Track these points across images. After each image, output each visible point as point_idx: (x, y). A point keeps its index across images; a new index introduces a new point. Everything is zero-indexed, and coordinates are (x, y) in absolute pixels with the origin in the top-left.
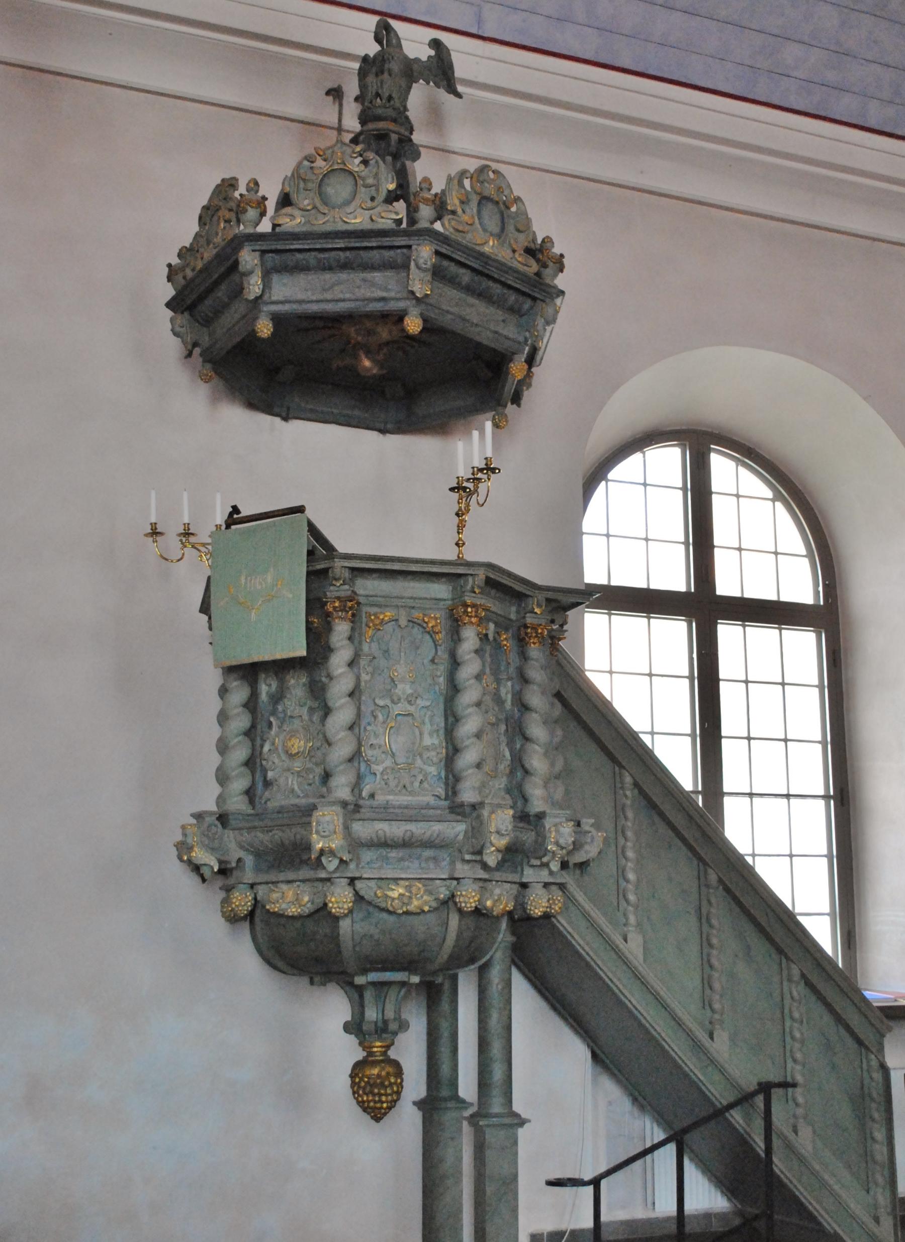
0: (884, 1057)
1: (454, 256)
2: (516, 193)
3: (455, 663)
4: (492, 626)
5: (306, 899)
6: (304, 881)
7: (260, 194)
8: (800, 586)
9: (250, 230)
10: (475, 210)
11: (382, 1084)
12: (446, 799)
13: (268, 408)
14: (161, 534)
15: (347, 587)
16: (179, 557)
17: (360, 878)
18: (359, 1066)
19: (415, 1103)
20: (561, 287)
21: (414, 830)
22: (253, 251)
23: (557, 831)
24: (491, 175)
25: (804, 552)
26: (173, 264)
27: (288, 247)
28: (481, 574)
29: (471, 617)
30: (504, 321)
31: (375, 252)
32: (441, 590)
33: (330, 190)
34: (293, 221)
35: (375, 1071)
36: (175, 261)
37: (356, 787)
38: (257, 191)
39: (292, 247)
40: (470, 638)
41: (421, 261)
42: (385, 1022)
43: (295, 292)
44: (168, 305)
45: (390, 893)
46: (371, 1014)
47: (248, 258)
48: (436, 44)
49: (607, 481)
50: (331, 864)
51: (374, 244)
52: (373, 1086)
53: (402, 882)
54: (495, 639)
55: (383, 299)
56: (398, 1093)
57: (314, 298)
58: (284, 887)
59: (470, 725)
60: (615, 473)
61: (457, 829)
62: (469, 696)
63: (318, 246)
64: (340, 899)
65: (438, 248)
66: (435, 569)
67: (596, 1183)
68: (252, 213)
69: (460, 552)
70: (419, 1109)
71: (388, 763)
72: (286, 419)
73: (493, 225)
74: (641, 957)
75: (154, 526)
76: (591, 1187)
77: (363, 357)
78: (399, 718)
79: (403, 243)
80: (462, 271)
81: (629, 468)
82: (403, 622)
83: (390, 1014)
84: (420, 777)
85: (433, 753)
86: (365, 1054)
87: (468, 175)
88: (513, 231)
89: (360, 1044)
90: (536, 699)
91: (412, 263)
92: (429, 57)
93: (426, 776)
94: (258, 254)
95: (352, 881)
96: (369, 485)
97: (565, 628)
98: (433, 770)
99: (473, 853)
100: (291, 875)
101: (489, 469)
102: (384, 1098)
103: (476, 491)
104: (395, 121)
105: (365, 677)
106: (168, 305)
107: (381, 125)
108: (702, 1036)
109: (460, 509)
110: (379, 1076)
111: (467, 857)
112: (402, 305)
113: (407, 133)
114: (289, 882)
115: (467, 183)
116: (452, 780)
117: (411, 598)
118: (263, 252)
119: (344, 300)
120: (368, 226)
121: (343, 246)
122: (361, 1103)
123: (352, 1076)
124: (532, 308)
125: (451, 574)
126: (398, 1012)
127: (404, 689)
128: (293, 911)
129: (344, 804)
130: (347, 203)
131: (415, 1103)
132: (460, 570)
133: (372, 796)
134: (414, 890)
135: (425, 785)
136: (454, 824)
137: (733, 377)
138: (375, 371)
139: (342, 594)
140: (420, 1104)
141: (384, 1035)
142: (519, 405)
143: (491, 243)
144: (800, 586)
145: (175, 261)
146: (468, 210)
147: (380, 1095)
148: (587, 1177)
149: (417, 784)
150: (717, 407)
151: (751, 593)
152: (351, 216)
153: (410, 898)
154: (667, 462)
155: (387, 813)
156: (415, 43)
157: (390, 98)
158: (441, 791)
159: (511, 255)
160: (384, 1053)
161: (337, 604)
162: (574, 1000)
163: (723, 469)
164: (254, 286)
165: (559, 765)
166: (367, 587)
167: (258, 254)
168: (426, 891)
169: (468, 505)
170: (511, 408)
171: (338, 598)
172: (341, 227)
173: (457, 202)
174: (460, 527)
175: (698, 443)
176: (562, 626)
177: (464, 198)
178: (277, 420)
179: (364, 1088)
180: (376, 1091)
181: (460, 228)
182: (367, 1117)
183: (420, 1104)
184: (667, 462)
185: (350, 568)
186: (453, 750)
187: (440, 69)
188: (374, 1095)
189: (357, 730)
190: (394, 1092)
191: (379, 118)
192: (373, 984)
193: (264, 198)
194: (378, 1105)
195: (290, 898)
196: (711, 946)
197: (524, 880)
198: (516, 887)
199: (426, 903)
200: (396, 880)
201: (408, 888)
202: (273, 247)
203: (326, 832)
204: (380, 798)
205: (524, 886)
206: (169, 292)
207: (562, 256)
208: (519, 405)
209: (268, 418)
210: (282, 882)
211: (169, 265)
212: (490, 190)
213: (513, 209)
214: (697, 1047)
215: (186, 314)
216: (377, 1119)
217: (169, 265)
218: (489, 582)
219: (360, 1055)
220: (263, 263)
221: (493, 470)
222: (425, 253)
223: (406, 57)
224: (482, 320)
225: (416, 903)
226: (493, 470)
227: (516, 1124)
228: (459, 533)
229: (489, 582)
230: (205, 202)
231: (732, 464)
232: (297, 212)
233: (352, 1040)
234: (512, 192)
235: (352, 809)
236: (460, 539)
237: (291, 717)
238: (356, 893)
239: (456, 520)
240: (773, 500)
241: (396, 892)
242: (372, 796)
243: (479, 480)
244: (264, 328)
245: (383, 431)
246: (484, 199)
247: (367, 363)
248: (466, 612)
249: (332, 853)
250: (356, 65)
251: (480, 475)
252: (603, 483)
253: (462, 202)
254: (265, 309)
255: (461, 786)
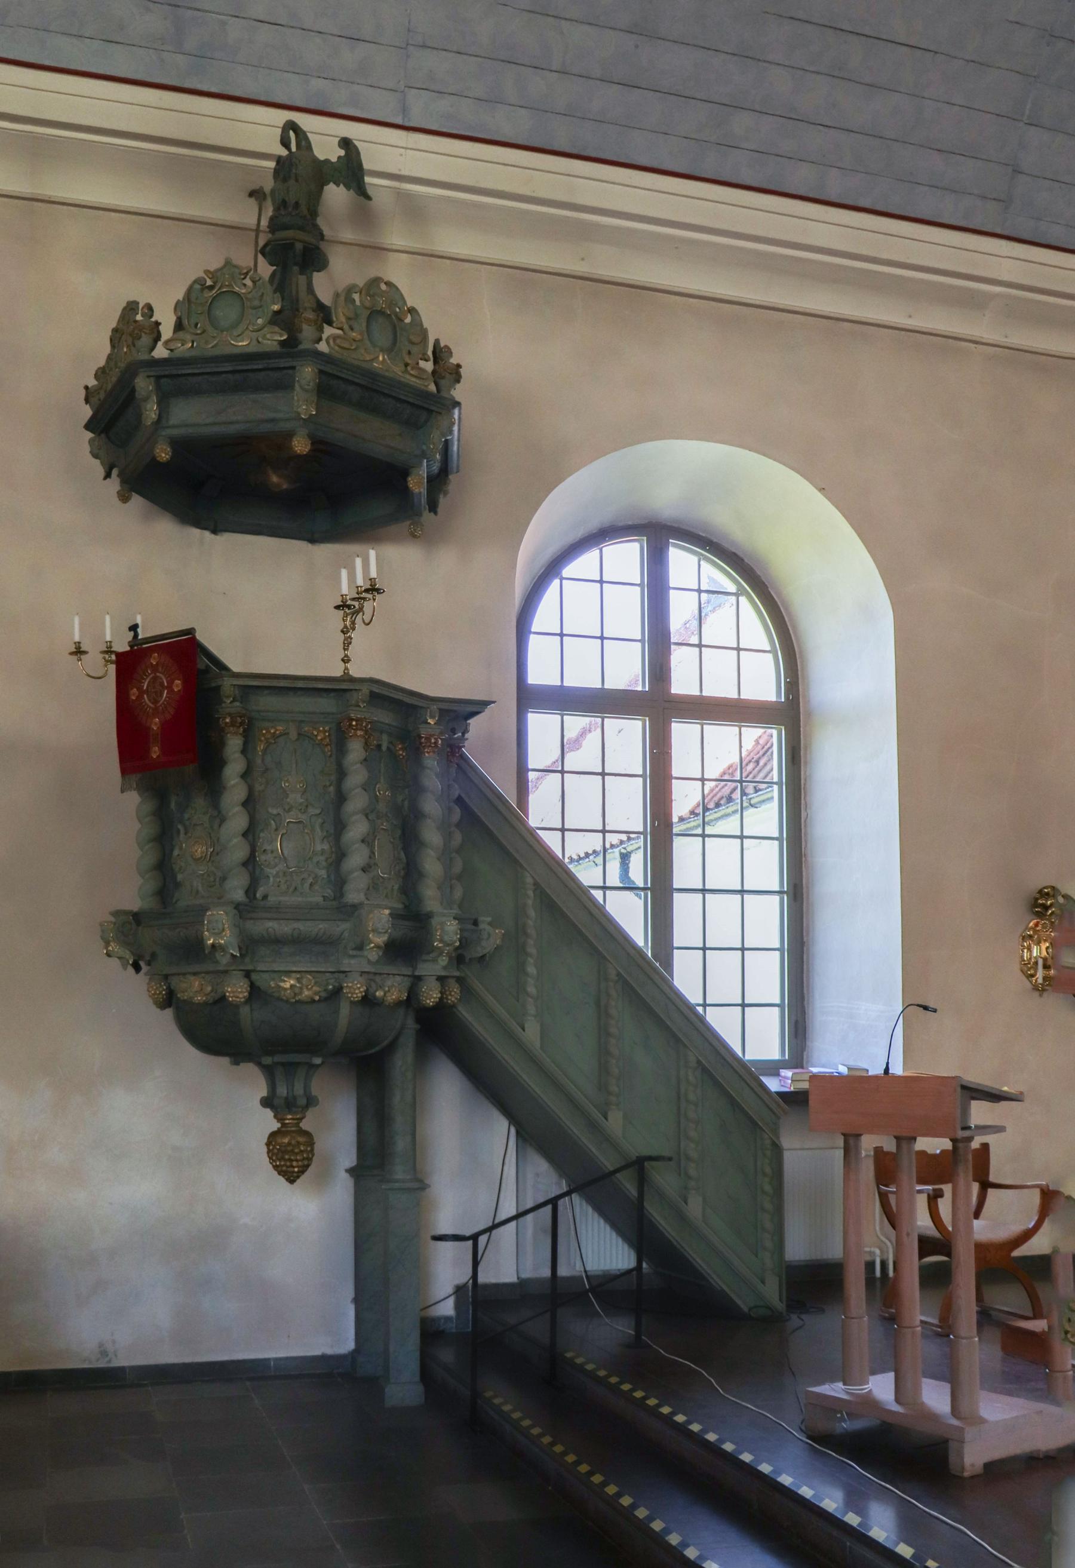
0: (778, 1138)
1: (339, 374)
2: (409, 304)
3: (342, 774)
4: (385, 737)
5: (209, 989)
6: (207, 973)
7: (153, 319)
8: (763, 683)
9: (144, 356)
10: (364, 324)
11: (292, 1151)
12: (335, 899)
13: (198, 524)
14: (85, 652)
15: (237, 704)
16: (100, 675)
17: (254, 971)
18: (273, 1135)
19: (347, 1171)
20: (457, 399)
21: (302, 928)
22: (148, 377)
23: (442, 929)
24: (383, 287)
25: (768, 648)
26: (90, 386)
27: (180, 372)
28: (365, 689)
29: (356, 730)
30: (400, 435)
31: (263, 373)
32: (326, 704)
33: (218, 313)
34: (184, 349)
35: (286, 1140)
36: (92, 382)
37: (250, 891)
38: (151, 316)
39: (184, 372)
40: (356, 751)
41: (303, 382)
42: (295, 1098)
43: (194, 416)
44: (88, 427)
45: (282, 984)
46: (282, 1091)
47: (143, 384)
48: (346, 143)
49: (562, 579)
50: (224, 960)
51: (260, 367)
52: (286, 1152)
53: (294, 975)
54: (388, 749)
55: (272, 420)
56: (310, 1159)
57: (207, 421)
58: (192, 978)
59: (357, 829)
60: (568, 571)
61: (343, 927)
62: (357, 802)
63: (208, 370)
64: (236, 990)
65: (322, 368)
66: (320, 686)
67: (475, 1238)
68: (145, 340)
69: (346, 668)
70: (351, 1176)
71: (282, 866)
72: (214, 532)
73: (382, 336)
74: (538, 1044)
75: (78, 645)
76: (470, 1242)
77: (270, 472)
78: (291, 825)
79: (287, 365)
80: (351, 388)
81: (585, 564)
82: (293, 735)
83: (299, 1090)
84: (310, 880)
85: (322, 858)
86: (279, 1125)
87: (357, 289)
88: (407, 343)
89: (275, 1117)
90: (431, 806)
91: (297, 385)
92: (339, 157)
93: (316, 877)
94: (152, 379)
95: (248, 974)
96: (267, 605)
97: (466, 736)
98: (323, 873)
99: (355, 949)
100: (197, 968)
101: (373, 589)
102: (295, 1164)
103: (361, 609)
104: (301, 228)
105: (258, 788)
106: (88, 427)
107: (290, 233)
108: (597, 1115)
109: (346, 627)
110: (289, 1144)
111: (351, 952)
112: (288, 426)
113: (313, 241)
114: (195, 974)
115: (356, 297)
116: (339, 883)
117: (301, 713)
118: (158, 378)
119: (237, 422)
120: (253, 349)
121: (230, 369)
122: (275, 1167)
123: (268, 1144)
124: (426, 421)
125: (339, 689)
126: (307, 1088)
127: (295, 798)
128: (199, 998)
129: (237, 906)
130: (235, 325)
131: (348, 1171)
132: (344, 686)
133: (265, 897)
134: (304, 981)
135: (316, 887)
136: (339, 923)
137: (681, 468)
138: (285, 486)
139: (232, 711)
140: (351, 1171)
141: (294, 1109)
142: (436, 513)
143: (381, 358)
144: (763, 683)
145: (92, 382)
146: (356, 326)
147: (291, 1160)
148: (468, 1233)
149: (307, 885)
150: (665, 500)
151: (711, 691)
152: (239, 339)
153: (301, 988)
154: (625, 557)
155: (278, 912)
156: (325, 138)
157: (297, 205)
158: (329, 892)
159: (403, 368)
160: (297, 1125)
161: (228, 720)
162: (490, 1085)
163: (683, 564)
164: (151, 411)
165: (458, 867)
166: (266, 703)
167: (152, 379)
168: (316, 983)
169: (353, 623)
170: (427, 516)
171: (230, 714)
172: (228, 351)
173: (343, 319)
174: (347, 644)
175: (658, 534)
176: (463, 734)
177: (351, 315)
178: (207, 533)
179: (277, 1155)
180: (287, 1157)
181: (346, 345)
182: (282, 1179)
183: (351, 1171)
184: (625, 557)
185: (239, 686)
186: (340, 855)
187: (350, 169)
188: (286, 1160)
189: (250, 837)
190: (304, 1159)
191: (286, 227)
192: (283, 1064)
193: (158, 324)
194: (291, 1169)
195: (195, 989)
196: (609, 1034)
197: (417, 973)
198: (410, 979)
199: (316, 993)
200: (288, 973)
201: (298, 980)
202: (167, 373)
203: (220, 931)
204: (272, 899)
205: (418, 979)
206: (87, 412)
207: (459, 366)
208: (436, 513)
209: (196, 532)
210: (190, 973)
211: (86, 388)
212: (381, 303)
213: (408, 320)
214: (593, 1126)
215: (103, 435)
216: (291, 1181)
217: (86, 388)
218: (373, 696)
219: (275, 1126)
220: (158, 387)
221: (378, 591)
222: (307, 373)
223: (315, 160)
224: (375, 436)
225: (306, 993)
226: (378, 591)
227: (418, 1189)
228: (345, 650)
229: (373, 696)
230: (114, 325)
231: (695, 559)
232: (188, 337)
233: (269, 1113)
234: (405, 303)
235: (244, 910)
236: (346, 656)
237: (195, 825)
238: (252, 985)
239: (342, 637)
240: (737, 595)
241: (289, 983)
242: (265, 897)
243: (364, 599)
244: (163, 453)
245: (312, 541)
246: (374, 314)
247: (275, 479)
248: (351, 725)
249: (223, 948)
250: (272, 164)
251: (364, 595)
252: (556, 582)
253: (349, 319)
254: (164, 433)
255: (349, 887)
